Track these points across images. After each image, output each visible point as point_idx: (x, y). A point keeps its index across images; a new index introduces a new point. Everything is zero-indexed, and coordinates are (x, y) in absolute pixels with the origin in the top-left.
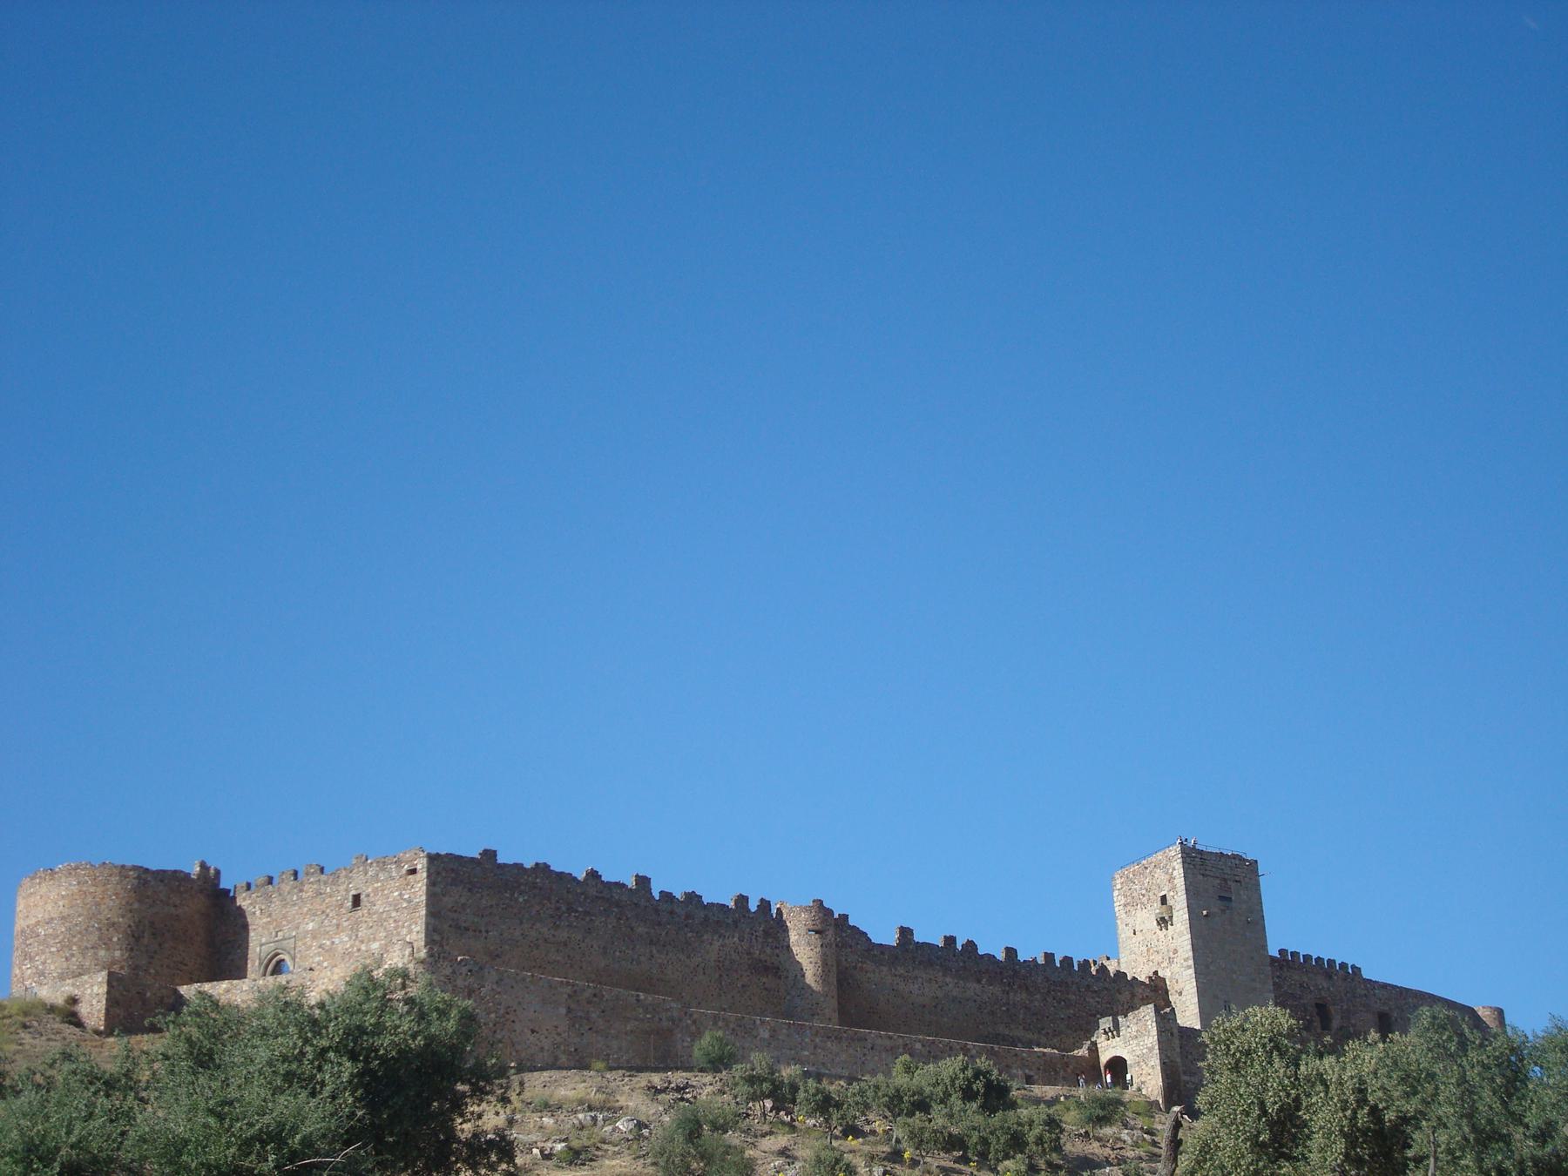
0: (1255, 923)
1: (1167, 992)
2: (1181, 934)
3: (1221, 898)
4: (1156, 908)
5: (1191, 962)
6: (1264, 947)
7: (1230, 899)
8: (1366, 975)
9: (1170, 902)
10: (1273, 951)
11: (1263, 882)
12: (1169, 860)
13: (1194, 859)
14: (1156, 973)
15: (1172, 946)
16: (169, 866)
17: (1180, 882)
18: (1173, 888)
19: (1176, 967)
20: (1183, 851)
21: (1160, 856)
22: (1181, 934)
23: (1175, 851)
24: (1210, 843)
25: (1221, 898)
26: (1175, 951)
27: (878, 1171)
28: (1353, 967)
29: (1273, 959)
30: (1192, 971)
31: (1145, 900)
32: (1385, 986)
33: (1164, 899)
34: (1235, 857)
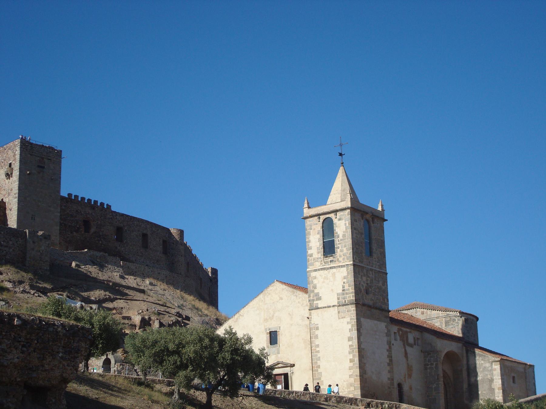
0: (56, 179)
1: (5, 209)
2: (15, 182)
3: (39, 166)
4: (6, 168)
5: (17, 195)
6: (59, 191)
7: (43, 167)
8: (113, 209)
9: (12, 166)
10: (64, 193)
11: (63, 161)
12: (15, 146)
13: (27, 147)
14: (2, 199)
15: (10, 187)
16: (47, 143)
17: (18, 157)
18: (15, 160)
19: (11, 198)
20: (21, 142)
21: (11, 144)
22: (15, 182)
23: (18, 142)
24: (39, 138)
25: (39, 166)
26: (12, 190)
27: (533, 407)
28: (107, 205)
29: (63, 198)
30: (16, 200)
31: (3, 164)
32: (123, 215)
33: (10, 164)
34: (49, 147)
